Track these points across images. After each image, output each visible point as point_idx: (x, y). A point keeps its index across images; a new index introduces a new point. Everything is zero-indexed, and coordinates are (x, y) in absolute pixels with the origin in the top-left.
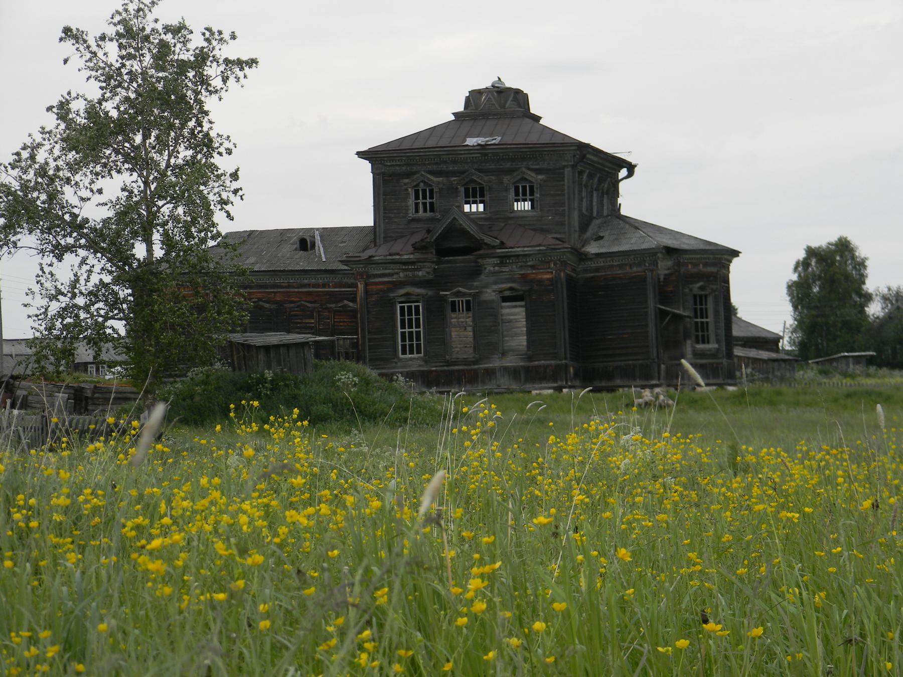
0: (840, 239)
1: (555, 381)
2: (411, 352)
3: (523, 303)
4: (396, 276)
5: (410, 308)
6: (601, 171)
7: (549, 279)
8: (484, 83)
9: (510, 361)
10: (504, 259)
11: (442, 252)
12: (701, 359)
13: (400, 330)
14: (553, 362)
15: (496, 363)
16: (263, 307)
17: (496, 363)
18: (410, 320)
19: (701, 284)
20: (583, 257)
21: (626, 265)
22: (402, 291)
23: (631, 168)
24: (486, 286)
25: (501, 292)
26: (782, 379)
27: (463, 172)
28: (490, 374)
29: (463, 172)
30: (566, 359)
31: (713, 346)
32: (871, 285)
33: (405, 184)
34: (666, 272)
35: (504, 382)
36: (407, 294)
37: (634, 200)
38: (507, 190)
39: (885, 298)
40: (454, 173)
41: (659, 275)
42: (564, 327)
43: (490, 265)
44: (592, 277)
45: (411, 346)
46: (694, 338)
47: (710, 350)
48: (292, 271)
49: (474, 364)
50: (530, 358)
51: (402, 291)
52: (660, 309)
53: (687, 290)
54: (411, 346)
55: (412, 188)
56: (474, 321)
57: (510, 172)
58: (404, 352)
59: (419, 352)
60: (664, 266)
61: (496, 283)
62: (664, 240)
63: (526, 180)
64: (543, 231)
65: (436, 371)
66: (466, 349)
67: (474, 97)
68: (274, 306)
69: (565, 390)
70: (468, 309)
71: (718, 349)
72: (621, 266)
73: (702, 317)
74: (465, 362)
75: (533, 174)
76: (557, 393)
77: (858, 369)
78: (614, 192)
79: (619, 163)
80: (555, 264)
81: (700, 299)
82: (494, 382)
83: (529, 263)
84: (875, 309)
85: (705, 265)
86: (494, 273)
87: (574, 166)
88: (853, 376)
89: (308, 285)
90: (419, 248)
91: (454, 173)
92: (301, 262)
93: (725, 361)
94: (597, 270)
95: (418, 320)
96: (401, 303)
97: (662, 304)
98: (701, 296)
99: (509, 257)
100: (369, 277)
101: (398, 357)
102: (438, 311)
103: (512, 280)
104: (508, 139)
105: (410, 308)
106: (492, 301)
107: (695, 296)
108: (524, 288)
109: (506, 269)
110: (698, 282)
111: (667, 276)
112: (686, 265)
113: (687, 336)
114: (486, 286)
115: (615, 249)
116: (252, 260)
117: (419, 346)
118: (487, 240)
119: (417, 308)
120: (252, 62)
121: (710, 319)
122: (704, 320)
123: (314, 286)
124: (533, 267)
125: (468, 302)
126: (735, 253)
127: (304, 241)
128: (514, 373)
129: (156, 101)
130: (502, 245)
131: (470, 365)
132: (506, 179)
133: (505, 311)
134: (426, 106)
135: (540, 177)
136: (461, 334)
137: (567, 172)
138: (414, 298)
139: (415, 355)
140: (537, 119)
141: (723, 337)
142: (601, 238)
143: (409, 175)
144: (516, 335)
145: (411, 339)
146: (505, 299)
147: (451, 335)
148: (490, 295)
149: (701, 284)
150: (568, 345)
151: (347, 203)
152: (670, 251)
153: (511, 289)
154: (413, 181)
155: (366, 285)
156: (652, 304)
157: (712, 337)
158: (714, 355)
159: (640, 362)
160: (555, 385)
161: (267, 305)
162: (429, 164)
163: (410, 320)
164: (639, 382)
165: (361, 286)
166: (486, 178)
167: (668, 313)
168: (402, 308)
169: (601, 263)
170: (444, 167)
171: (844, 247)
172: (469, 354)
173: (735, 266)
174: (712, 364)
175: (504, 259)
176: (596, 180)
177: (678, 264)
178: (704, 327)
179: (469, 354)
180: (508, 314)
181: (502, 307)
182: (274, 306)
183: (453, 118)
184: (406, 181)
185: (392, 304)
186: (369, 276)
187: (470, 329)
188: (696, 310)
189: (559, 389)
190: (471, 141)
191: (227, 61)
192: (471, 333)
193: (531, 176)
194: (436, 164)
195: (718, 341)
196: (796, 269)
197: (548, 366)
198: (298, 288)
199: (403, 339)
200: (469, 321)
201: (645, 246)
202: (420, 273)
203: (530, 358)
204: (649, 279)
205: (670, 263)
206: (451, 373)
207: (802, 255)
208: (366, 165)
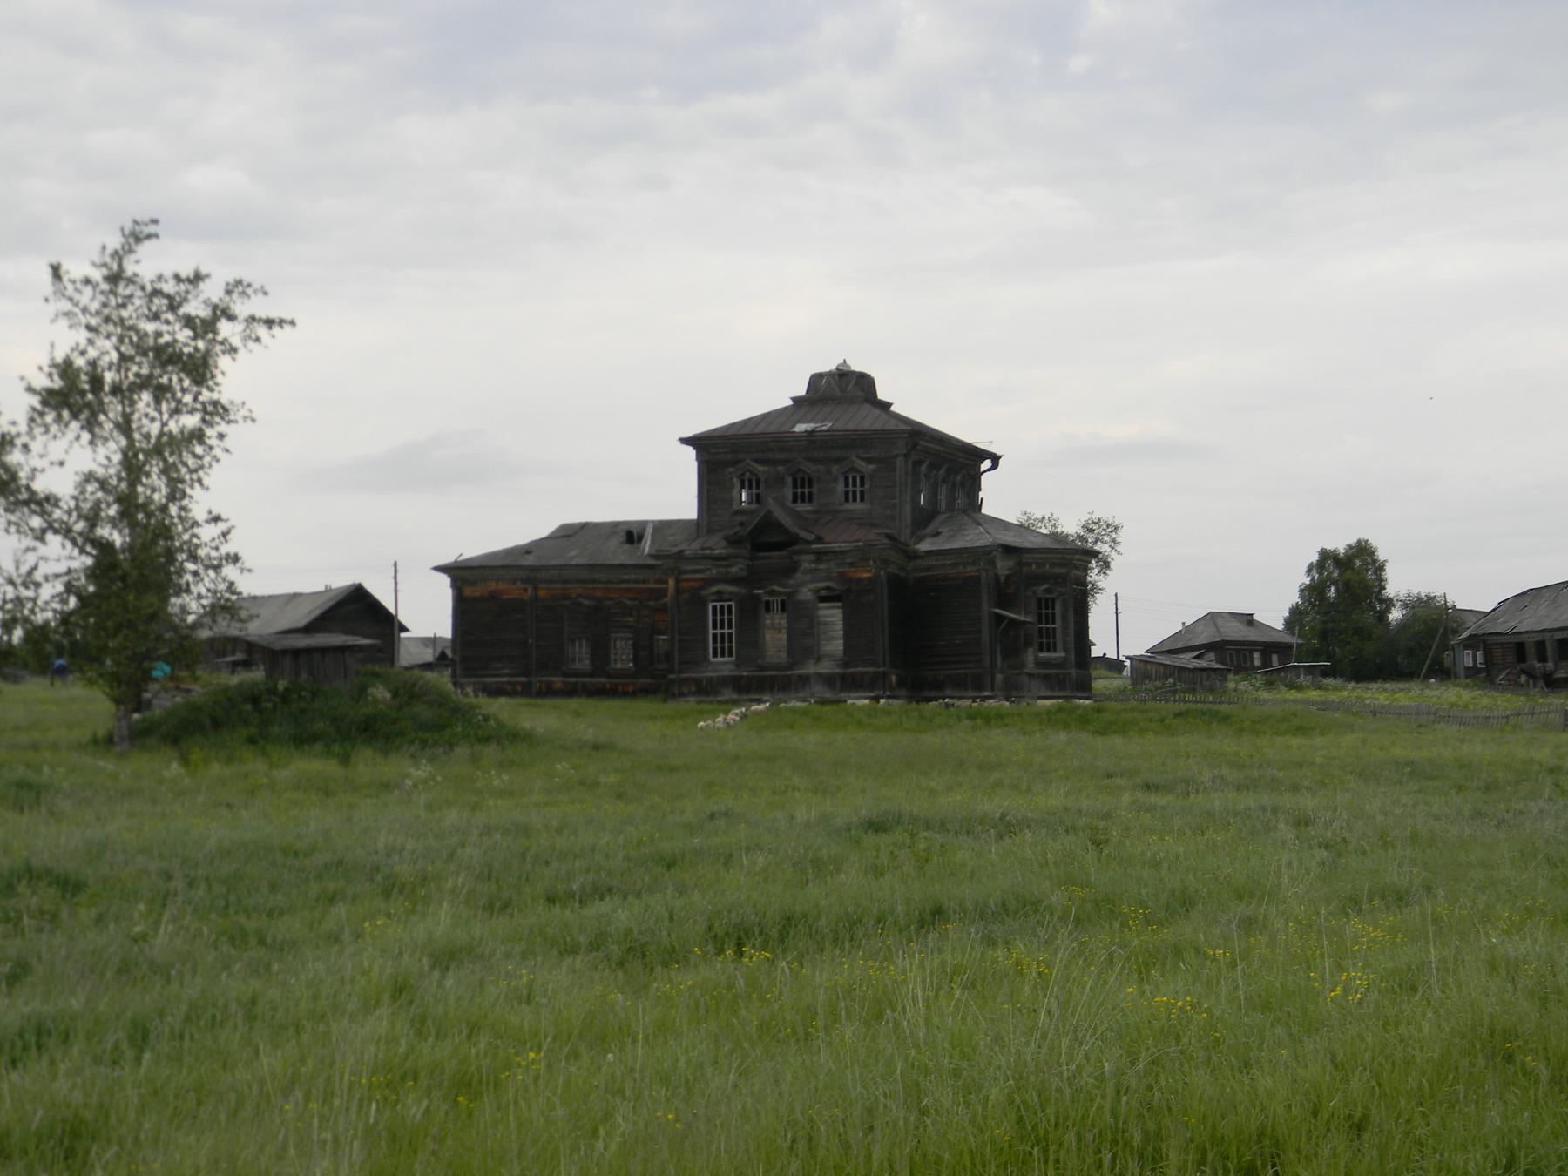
0: (1359, 541)
2: (723, 655)
5: (722, 607)
6: (957, 466)
7: (869, 579)
8: (829, 366)
9: (826, 667)
10: (820, 555)
11: (758, 547)
13: (711, 631)
14: (871, 669)
15: (810, 669)
17: (810, 669)
18: (722, 621)
20: (914, 556)
22: (714, 589)
23: (995, 459)
25: (817, 591)
26: (1211, 690)
28: (804, 680)
29: (738, 462)
31: (1060, 654)
32: (1391, 590)
35: (819, 690)
36: (719, 592)
37: (1000, 498)
38: (835, 480)
39: (1405, 605)
40: (781, 462)
41: (997, 575)
43: (806, 562)
45: (723, 649)
50: (846, 664)
51: (714, 589)
54: (723, 649)
56: (789, 623)
57: (838, 461)
58: (715, 655)
59: (730, 655)
60: (1003, 566)
61: (812, 582)
63: (857, 471)
64: (873, 525)
67: (816, 379)
70: (783, 609)
71: (1066, 659)
72: (955, 565)
74: (777, 667)
77: (1304, 679)
78: (976, 486)
79: (981, 455)
81: (1046, 604)
84: (1395, 615)
85: (1053, 565)
86: (812, 571)
87: (906, 456)
88: (1299, 688)
89: (627, 581)
90: (734, 541)
91: (781, 462)
92: (623, 556)
93: (1073, 672)
94: (928, 568)
95: (730, 621)
98: (1047, 600)
99: (826, 553)
100: (680, 572)
102: (751, 612)
103: (828, 579)
104: (839, 426)
107: (1039, 600)
111: (1008, 577)
112: (1029, 565)
113: (1028, 644)
114: (802, 584)
115: (947, 546)
116: (574, 553)
117: (730, 649)
118: (803, 534)
119: (730, 607)
120: (292, 323)
121: (1058, 625)
122: (718, 631)
123: (636, 582)
124: (851, 564)
125: (783, 603)
127: (631, 534)
129: (150, 367)
130: (819, 540)
132: (835, 469)
133: (821, 612)
134: (764, 388)
135: (871, 467)
136: (775, 637)
137: (899, 462)
139: (726, 659)
140: (885, 406)
141: (1072, 645)
142: (938, 534)
143: (734, 463)
144: (833, 638)
145: (723, 641)
146: (823, 599)
148: (806, 594)
151: (670, 493)
152: (1008, 550)
153: (827, 588)
155: (677, 582)
157: (1059, 645)
158: (1061, 664)
161: (586, 602)
163: (722, 621)
165: (671, 583)
166: (814, 468)
168: (714, 608)
169: (932, 562)
171: (1363, 551)
172: (783, 657)
175: (820, 555)
176: (942, 471)
177: (1020, 564)
178: (1051, 633)
179: (783, 657)
185: (704, 604)
186: (680, 572)
188: (1040, 615)
189: (876, 699)
190: (800, 428)
191: (252, 319)
193: (862, 465)
195: (1066, 650)
196: (1309, 571)
199: (715, 641)
200: (784, 622)
201: (977, 544)
202: (733, 570)
204: (983, 580)
205: (1011, 563)
207: (1315, 558)
208: (690, 453)
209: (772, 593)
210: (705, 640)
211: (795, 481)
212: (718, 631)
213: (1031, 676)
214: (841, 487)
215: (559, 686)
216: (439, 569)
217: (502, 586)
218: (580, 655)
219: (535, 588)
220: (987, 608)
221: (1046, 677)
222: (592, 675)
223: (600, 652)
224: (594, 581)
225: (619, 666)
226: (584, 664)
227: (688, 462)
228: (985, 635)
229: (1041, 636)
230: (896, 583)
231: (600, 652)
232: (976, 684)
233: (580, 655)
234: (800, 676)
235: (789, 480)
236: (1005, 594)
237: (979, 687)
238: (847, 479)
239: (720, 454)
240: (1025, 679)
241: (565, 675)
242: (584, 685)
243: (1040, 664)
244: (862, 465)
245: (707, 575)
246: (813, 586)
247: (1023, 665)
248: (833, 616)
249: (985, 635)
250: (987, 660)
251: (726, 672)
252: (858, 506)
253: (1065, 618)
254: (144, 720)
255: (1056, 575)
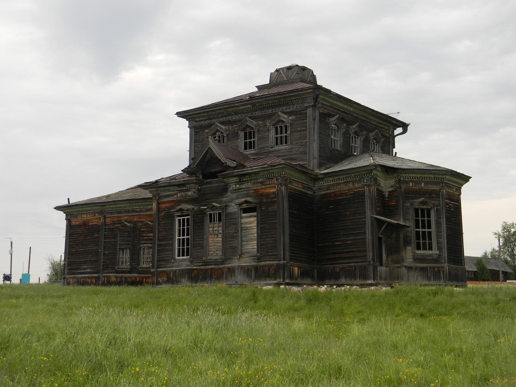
1: (275, 279)
3: (255, 214)
4: (175, 196)
5: (184, 220)
6: (382, 129)
7: (274, 193)
9: (246, 262)
12: (421, 263)
13: (177, 238)
15: (235, 263)
16: (126, 225)
17: (235, 263)
19: (422, 199)
21: (349, 182)
24: (231, 201)
25: (240, 205)
27: (240, 121)
28: (231, 271)
29: (211, 125)
30: (284, 259)
31: (435, 252)
33: (207, 133)
34: (390, 189)
35: (240, 277)
37: (408, 149)
42: (284, 232)
43: (233, 184)
44: (326, 194)
46: (414, 245)
47: (430, 255)
48: (138, 199)
49: (221, 265)
52: (376, 219)
53: (408, 204)
55: (211, 135)
57: (270, 116)
59: (187, 255)
61: (237, 198)
62: (389, 163)
63: (283, 122)
65: (196, 269)
66: (218, 252)
68: (132, 225)
69: (282, 287)
70: (220, 220)
73: (423, 227)
74: (216, 262)
75: (286, 117)
76: (275, 289)
80: (277, 180)
81: (422, 216)
82: (233, 278)
83: (259, 180)
85: (427, 183)
91: (235, 122)
94: (328, 188)
96: (179, 216)
97: (378, 214)
98: (423, 210)
99: (244, 175)
100: (160, 197)
101: (175, 259)
102: (197, 224)
103: (248, 195)
105: (184, 220)
106: (234, 213)
107: (416, 210)
108: (255, 201)
109: (244, 186)
110: (419, 198)
112: (408, 182)
113: (407, 243)
124: (262, 183)
125: (220, 214)
126: (466, 179)
128: (247, 271)
131: (218, 265)
132: (268, 123)
133: (244, 220)
135: (291, 118)
136: (214, 242)
137: (309, 111)
138: (185, 213)
146: (245, 211)
147: (208, 241)
149: (422, 199)
150: (287, 249)
153: (246, 202)
154: (211, 130)
155: (158, 204)
156: (370, 215)
157: (434, 245)
158: (437, 260)
159: (360, 264)
160: (275, 282)
162: (221, 117)
164: (359, 281)
165: (154, 205)
167: (384, 222)
168: (179, 220)
170: (230, 118)
173: (465, 189)
174: (434, 268)
180: (246, 223)
181: (241, 218)
182: (132, 225)
183: (256, 90)
184: (207, 131)
185: (172, 217)
186: (160, 197)
187: (220, 236)
188: (417, 222)
192: (221, 239)
193: (284, 117)
194: (225, 116)
197: (272, 265)
198: (145, 212)
202: (190, 193)
203: (259, 259)
204: (367, 193)
205: (392, 182)
206: (206, 270)
208: (185, 123)
209: (213, 208)
210: (172, 245)
211: (245, 134)
212: (181, 237)
213: (409, 268)
214: (272, 134)
215: (113, 279)
216: (58, 208)
217: (89, 217)
218: (125, 258)
219: (105, 217)
220: (370, 215)
221: (422, 269)
222: (130, 272)
223: (135, 258)
224: (133, 211)
225: (145, 266)
226: (126, 266)
227: (183, 129)
228: (369, 236)
229: (418, 238)
230: (297, 200)
231: (135, 258)
232: (361, 275)
233: (125, 258)
234: (229, 269)
235: (242, 134)
236: (386, 205)
237: (365, 277)
238: (277, 128)
239: (202, 120)
240: (404, 271)
241: (117, 272)
242: (126, 278)
243: (416, 259)
244: (284, 117)
245: (174, 198)
246: (237, 201)
247: (403, 260)
248: (250, 222)
249: (369, 236)
250: (370, 255)
251: (184, 266)
252: (284, 147)
253: (438, 224)
254: (386, 290)
255: (438, 194)
